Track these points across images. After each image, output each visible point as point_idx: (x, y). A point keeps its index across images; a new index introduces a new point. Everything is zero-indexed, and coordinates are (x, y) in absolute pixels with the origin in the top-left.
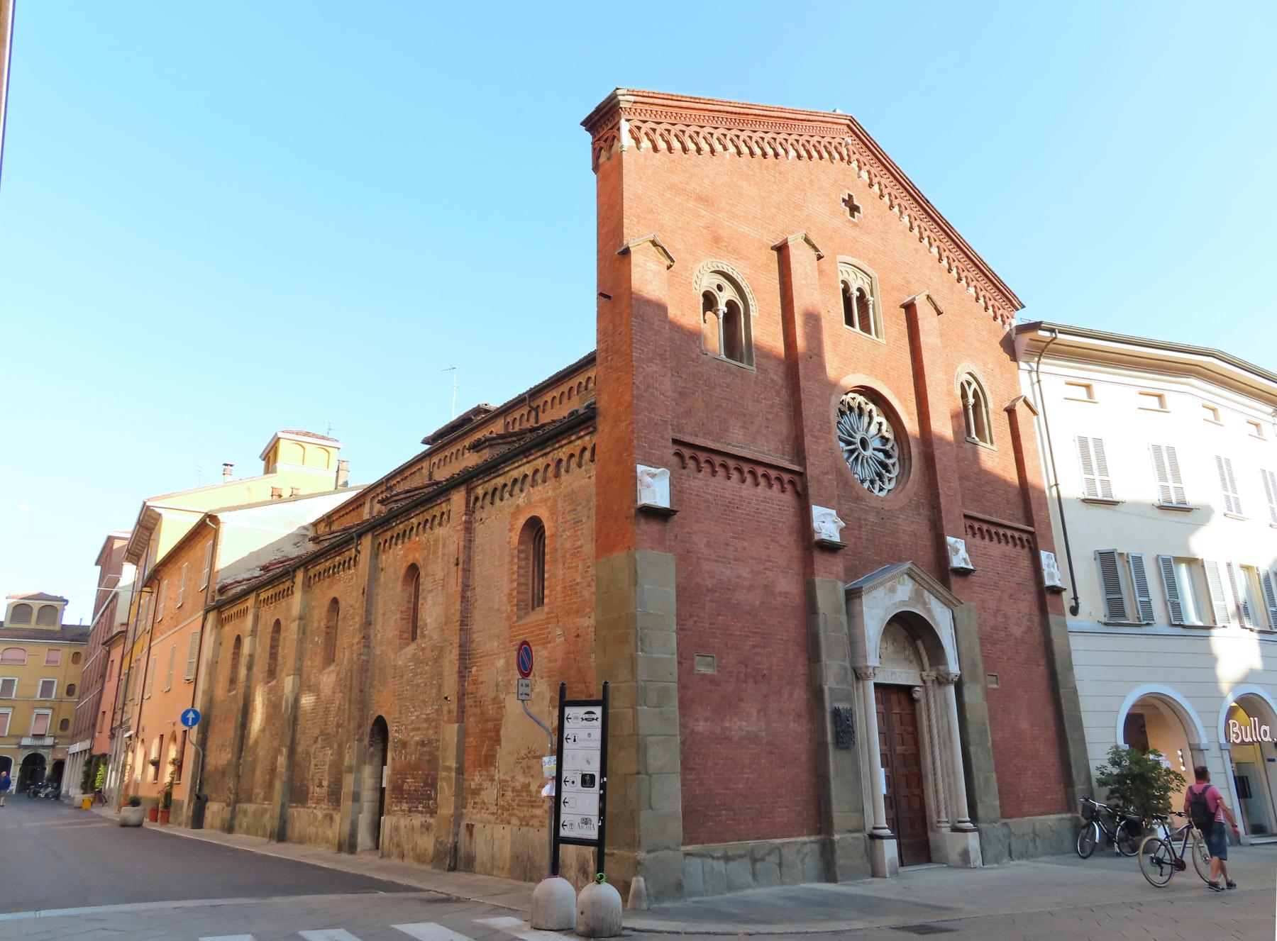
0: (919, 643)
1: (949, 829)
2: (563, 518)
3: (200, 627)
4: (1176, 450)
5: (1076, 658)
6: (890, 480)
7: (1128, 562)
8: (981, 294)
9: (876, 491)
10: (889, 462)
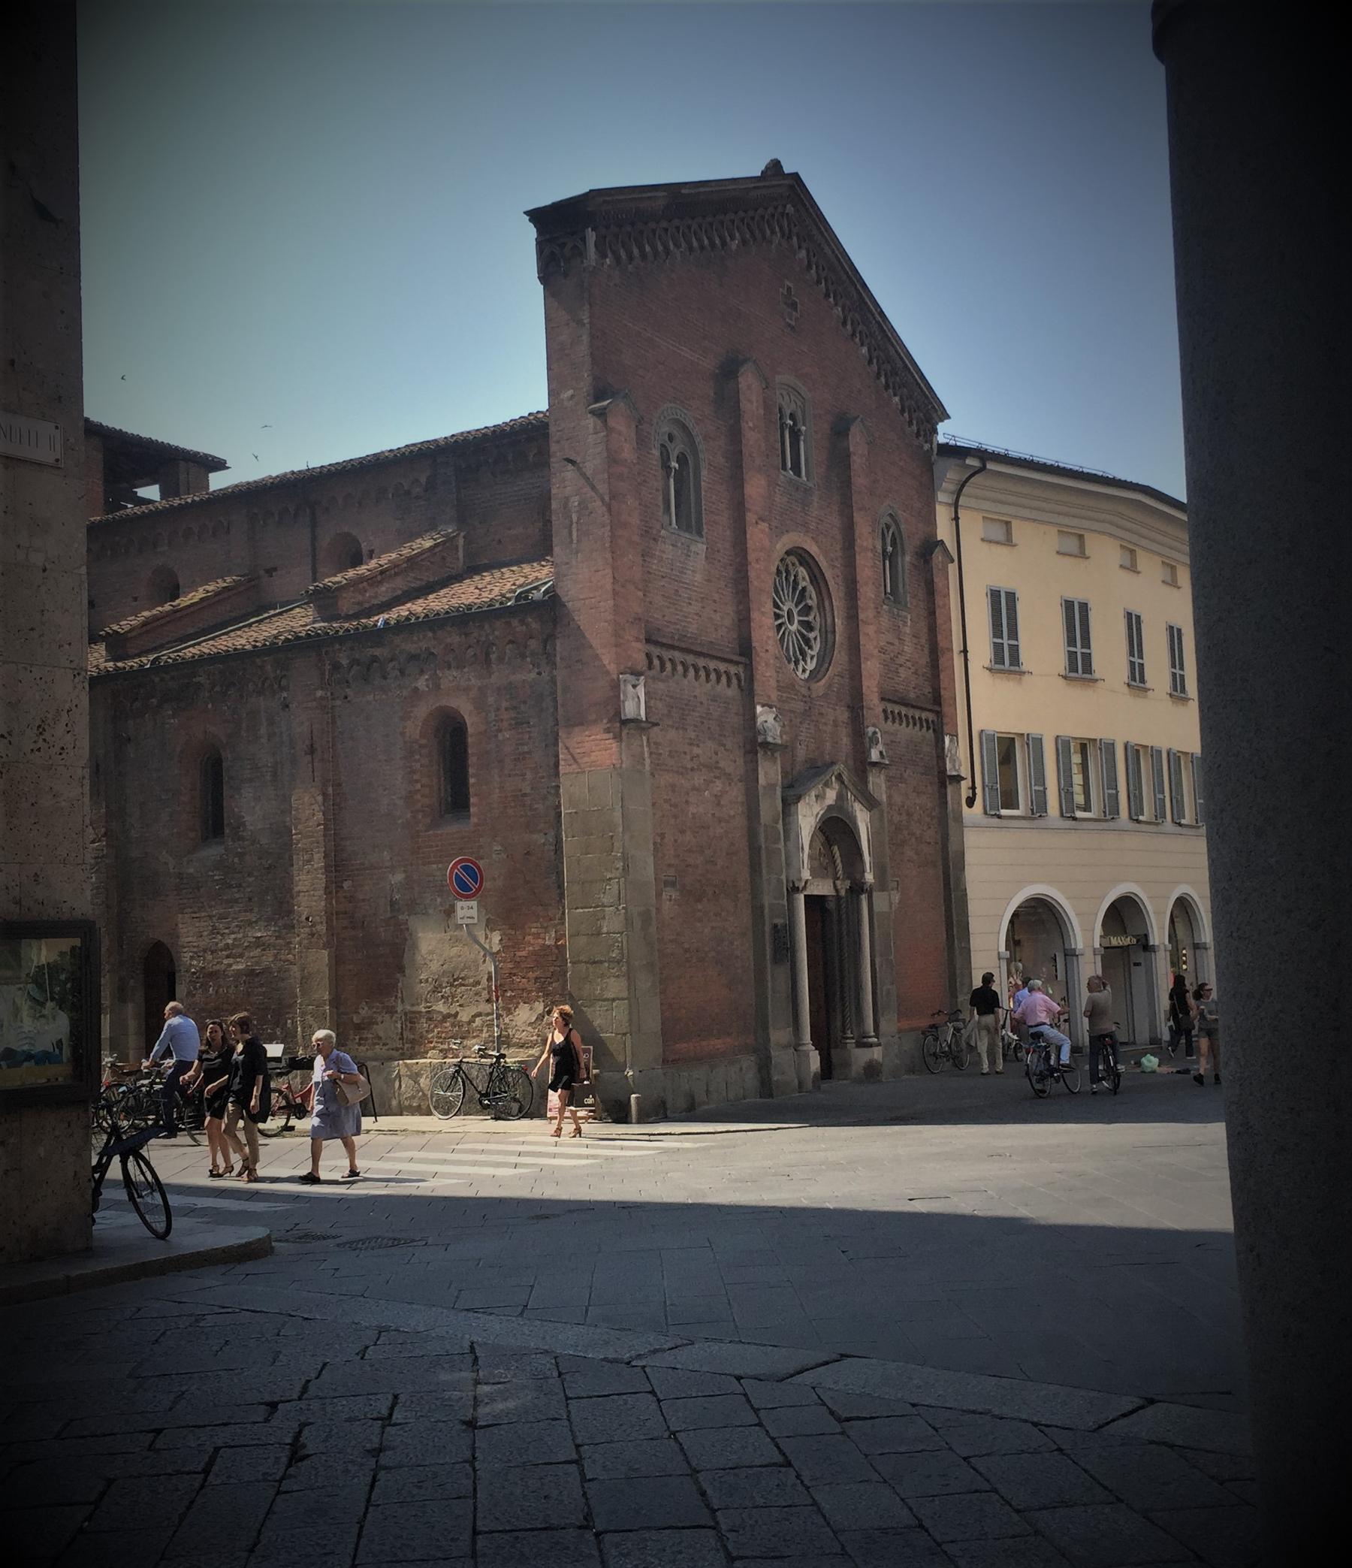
0: (836, 849)
1: (854, 1045)
2: (496, 716)
3: (1065, 991)
4: (1089, 606)
5: (970, 857)
6: (812, 657)
7: (1028, 744)
8: (875, 354)
9: (799, 673)
10: (812, 635)
